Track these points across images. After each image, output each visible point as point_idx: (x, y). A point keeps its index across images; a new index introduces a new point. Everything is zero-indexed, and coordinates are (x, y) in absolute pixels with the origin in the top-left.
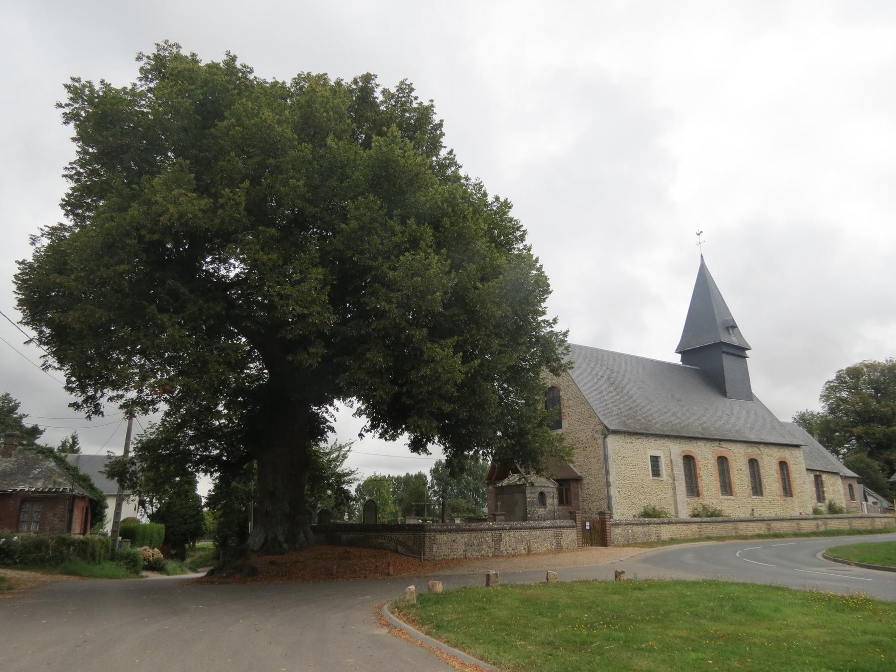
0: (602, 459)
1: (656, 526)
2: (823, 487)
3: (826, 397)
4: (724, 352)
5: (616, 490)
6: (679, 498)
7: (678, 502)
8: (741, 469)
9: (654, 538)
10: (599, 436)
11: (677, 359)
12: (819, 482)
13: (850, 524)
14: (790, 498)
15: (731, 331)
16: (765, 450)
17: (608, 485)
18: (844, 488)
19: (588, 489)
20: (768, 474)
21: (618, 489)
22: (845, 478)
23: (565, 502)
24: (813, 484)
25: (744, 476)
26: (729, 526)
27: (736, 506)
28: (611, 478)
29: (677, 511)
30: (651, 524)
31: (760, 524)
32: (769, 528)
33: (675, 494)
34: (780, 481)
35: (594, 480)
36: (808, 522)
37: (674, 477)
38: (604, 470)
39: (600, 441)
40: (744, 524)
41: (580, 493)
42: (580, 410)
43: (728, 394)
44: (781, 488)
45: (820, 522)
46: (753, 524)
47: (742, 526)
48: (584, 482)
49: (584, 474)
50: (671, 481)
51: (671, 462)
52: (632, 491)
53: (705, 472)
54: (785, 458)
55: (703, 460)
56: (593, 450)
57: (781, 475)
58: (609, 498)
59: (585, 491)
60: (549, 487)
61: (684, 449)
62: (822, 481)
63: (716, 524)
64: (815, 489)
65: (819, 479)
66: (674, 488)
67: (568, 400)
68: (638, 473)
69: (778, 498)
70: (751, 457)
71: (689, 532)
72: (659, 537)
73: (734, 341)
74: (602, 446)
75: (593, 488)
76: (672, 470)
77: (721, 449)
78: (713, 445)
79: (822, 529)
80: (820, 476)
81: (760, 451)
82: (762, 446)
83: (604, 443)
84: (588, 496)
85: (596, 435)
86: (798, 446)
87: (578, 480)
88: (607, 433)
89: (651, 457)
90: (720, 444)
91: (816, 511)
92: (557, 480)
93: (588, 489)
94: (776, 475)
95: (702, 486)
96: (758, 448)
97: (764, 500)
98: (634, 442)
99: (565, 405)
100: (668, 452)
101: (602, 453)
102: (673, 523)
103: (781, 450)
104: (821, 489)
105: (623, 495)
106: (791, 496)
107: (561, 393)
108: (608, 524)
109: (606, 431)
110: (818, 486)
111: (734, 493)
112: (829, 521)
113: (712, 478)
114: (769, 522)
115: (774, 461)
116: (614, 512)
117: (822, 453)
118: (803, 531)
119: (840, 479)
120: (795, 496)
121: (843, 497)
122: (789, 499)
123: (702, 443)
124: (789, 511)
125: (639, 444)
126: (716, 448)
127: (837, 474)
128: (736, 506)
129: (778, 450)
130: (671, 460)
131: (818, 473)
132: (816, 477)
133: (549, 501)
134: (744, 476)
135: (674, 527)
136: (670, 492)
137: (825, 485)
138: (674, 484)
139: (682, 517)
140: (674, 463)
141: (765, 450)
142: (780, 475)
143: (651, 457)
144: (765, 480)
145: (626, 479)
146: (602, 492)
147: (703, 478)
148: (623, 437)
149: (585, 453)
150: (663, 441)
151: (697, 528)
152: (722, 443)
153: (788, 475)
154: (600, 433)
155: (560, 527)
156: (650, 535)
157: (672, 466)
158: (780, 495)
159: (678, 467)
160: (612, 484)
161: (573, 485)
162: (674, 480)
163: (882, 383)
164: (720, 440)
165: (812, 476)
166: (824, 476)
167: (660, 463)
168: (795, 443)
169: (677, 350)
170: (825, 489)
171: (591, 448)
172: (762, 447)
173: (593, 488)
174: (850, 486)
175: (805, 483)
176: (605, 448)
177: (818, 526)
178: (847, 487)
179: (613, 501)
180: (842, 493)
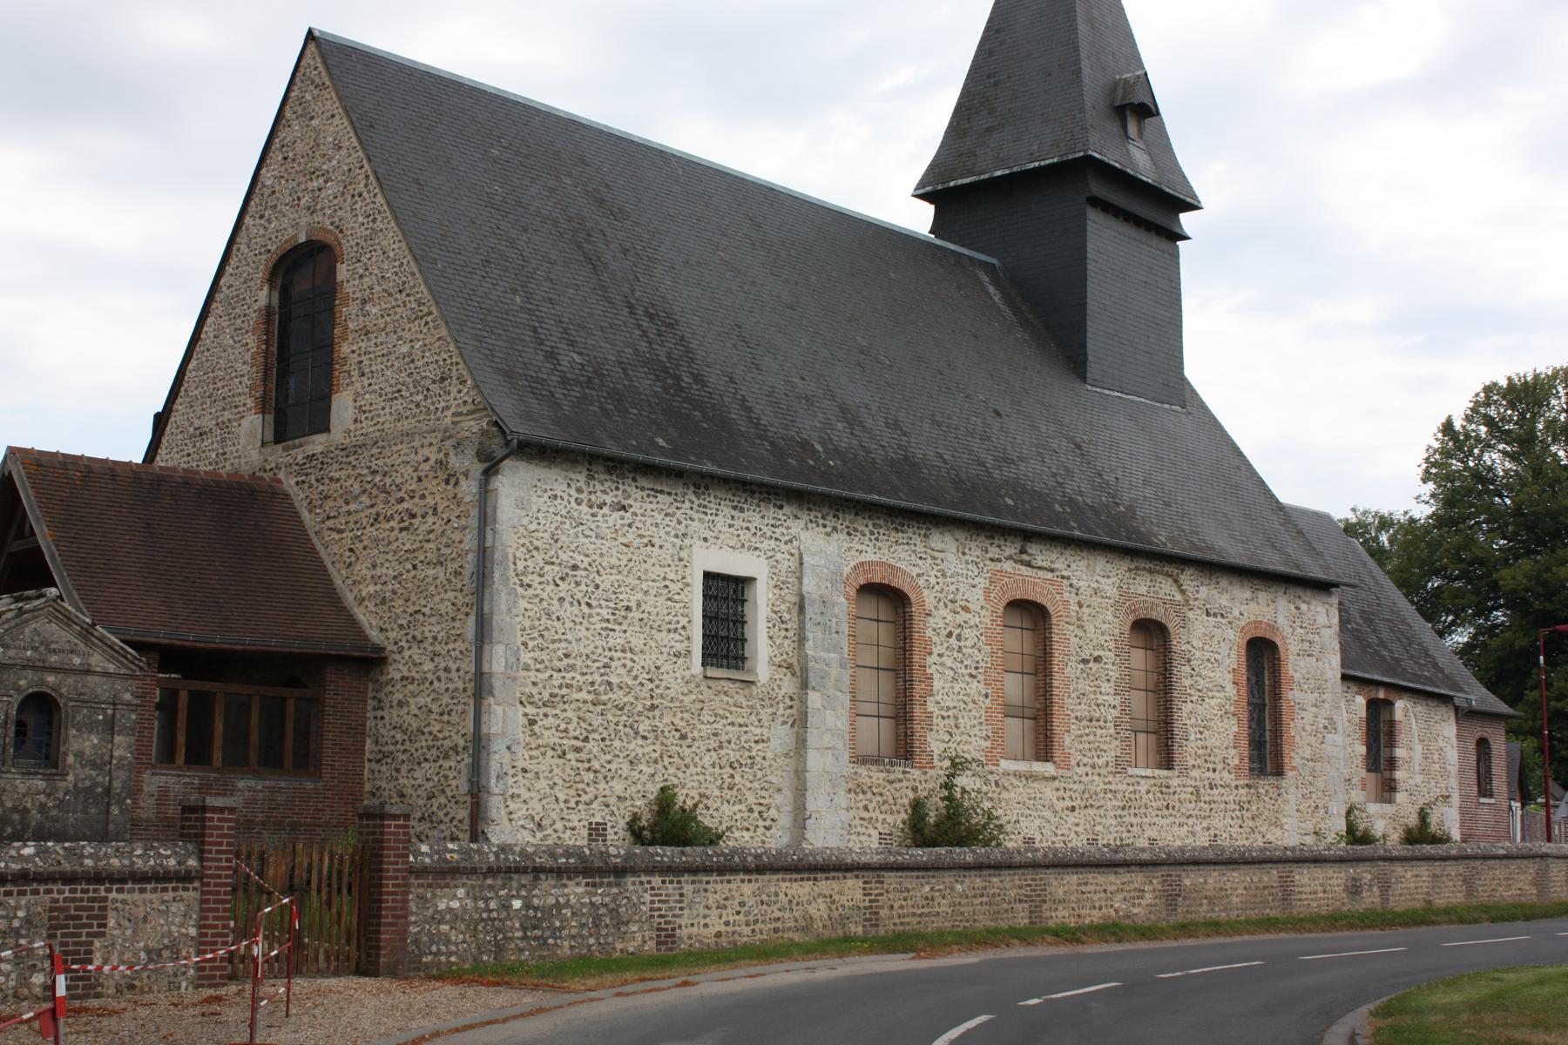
0: (468, 571)
1: (656, 880)
2: (1392, 742)
3: (1435, 470)
4: (1095, 202)
5: (518, 716)
6: (816, 762)
7: (810, 777)
8: (1097, 659)
9: (639, 939)
10: (466, 462)
11: (919, 219)
12: (1383, 728)
13: (1468, 881)
14: (1271, 780)
15: (1132, 129)
16: (1203, 591)
17: (481, 686)
18: (1462, 752)
19: (400, 704)
20: (1202, 683)
21: (530, 710)
22: (1466, 715)
23: (288, 757)
24: (1360, 733)
25: (1106, 688)
26: (1009, 885)
27: (1060, 805)
28: (497, 660)
29: (801, 818)
30: (634, 871)
31: (1137, 878)
32: (1171, 897)
33: (801, 743)
34: (1244, 716)
35: (428, 666)
36: (1320, 873)
37: (805, 670)
38: (471, 622)
39: (469, 488)
40: (1072, 879)
41: (370, 723)
42: (405, 349)
43: (1093, 370)
44: (1244, 743)
45: (1366, 873)
46: (1111, 880)
47: (1063, 885)
48: (395, 671)
49: (392, 635)
50: (789, 686)
51: (802, 609)
52: (597, 721)
53: (949, 662)
54: (1273, 627)
55: (943, 612)
56: (438, 528)
57: (1251, 692)
58: (478, 745)
59: (392, 715)
60: (88, 672)
61: (862, 558)
62: (1392, 723)
63: (948, 877)
64: (1363, 750)
65: (1384, 716)
66: (801, 722)
67: (364, 302)
68: (637, 642)
69: (1228, 777)
70: (1143, 614)
71: (819, 910)
72: (667, 937)
73: (1139, 163)
74: (474, 512)
75: (421, 700)
76: (802, 640)
77: (1024, 570)
78: (994, 552)
79: (1370, 898)
80: (1389, 704)
81: (1183, 592)
82: (1189, 572)
83: (485, 494)
84: (399, 737)
85: (455, 462)
86: (1322, 587)
87: (370, 662)
88: (499, 453)
89: (708, 576)
90: (1023, 551)
91: (1356, 836)
92: (168, 657)
93: (400, 704)
94: (1231, 690)
95: (930, 715)
96: (1176, 581)
97: (1174, 782)
98: (636, 507)
99: (352, 326)
100: (794, 564)
101: (469, 542)
102: (746, 870)
103: (1263, 596)
104: (1384, 753)
105: (550, 737)
106: (1279, 772)
107: (342, 272)
108: (391, 867)
109: (499, 440)
110: (1377, 740)
111: (1057, 753)
112: (1399, 869)
113: (975, 687)
114: (1175, 872)
115: (1231, 634)
116: (493, 813)
117: (1403, 621)
118: (1298, 910)
119: (1452, 715)
120: (1290, 774)
121: (1454, 782)
122: (1265, 785)
123: (948, 538)
124: (1263, 829)
125: (659, 517)
126: (1008, 566)
127: (1445, 699)
128: (1060, 805)
129: (1248, 594)
130: (802, 598)
131: (1381, 695)
132: (1372, 704)
133: (81, 743)
134: (1106, 688)
135: (747, 889)
136: (780, 737)
137: (1402, 738)
138: (803, 701)
139: (819, 844)
140: (809, 611)
141: (1203, 589)
142: (1244, 691)
143: (708, 576)
144: (1187, 708)
145: (572, 667)
146: (454, 718)
147: (937, 684)
148: (581, 478)
149: (407, 541)
150: (771, 512)
151: (859, 895)
152: (1033, 549)
153: (1276, 695)
154: (470, 452)
155: (98, 878)
156: (620, 922)
157: (802, 628)
158: (1237, 768)
159: (827, 630)
160: (497, 684)
161: (336, 688)
162: (805, 685)
163: (1339, 842)
164: (1028, 536)
165: (1361, 701)
166: (1401, 706)
167: (748, 609)
168: (1316, 573)
169: (921, 185)
170: (1400, 752)
171: (430, 519)
172: (1188, 578)
173: (421, 700)
174: (1483, 745)
175: (1331, 725)
176: (486, 519)
177: (1354, 889)
178: (1472, 746)
179: (498, 759)
180: (1453, 770)
